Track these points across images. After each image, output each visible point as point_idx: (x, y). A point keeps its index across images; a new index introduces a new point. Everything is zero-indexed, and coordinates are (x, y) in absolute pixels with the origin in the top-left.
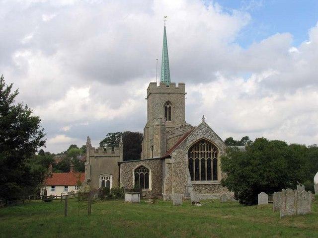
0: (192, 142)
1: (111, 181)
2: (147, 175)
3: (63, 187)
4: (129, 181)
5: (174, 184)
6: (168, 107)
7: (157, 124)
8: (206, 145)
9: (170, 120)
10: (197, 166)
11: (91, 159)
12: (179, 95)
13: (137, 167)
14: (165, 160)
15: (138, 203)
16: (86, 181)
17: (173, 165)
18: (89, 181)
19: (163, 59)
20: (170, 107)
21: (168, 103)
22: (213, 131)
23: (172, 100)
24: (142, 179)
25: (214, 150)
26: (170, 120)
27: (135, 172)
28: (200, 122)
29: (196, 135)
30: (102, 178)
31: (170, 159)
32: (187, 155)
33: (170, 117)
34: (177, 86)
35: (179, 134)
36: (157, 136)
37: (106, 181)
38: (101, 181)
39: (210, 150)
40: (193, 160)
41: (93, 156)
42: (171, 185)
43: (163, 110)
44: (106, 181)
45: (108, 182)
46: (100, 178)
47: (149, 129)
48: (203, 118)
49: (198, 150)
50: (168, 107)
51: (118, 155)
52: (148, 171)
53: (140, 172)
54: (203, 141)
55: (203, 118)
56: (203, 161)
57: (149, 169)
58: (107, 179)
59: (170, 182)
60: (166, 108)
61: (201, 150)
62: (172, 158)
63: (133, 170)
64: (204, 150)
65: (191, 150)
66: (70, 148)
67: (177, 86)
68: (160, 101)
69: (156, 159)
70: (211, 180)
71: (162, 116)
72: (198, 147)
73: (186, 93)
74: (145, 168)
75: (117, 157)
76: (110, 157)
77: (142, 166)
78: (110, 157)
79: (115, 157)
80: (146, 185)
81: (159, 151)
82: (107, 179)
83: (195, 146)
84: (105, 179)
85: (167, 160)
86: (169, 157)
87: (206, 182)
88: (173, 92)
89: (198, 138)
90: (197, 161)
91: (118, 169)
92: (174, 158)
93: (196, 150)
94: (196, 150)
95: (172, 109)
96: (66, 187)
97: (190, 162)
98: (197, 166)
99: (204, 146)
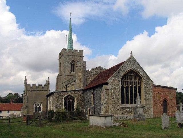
0: (124, 72)
1: (42, 107)
2: (73, 102)
3: (7, 111)
4: (60, 106)
5: (111, 107)
6: (73, 64)
7: (80, 65)
8: (133, 75)
9: (74, 71)
10: (127, 92)
11: (27, 92)
12: (80, 57)
13: (66, 96)
14: (102, 86)
15: (111, 127)
16: (24, 106)
17: (110, 91)
18: (27, 107)
19: (70, 35)
20: (74, 64)
21: (73, 61)
22: (139, 64)
23: (75, 60)
24: (69, 104)
25: (139, 80)
26: (74, 71)
27: (65, 99)
28: (129, 56)
29: (127, 67)
30: (35, 105)
31: (106, 86)
32: (120, 82)
33: (74, 70)
34: (78, 52)
35: (95, 73)
36: (80, 74)
37: (38, 107)
38: (34, 107)
39: (136, 80)
40: (133, 87)
41: (29, 90)
42: (108, 108)
43: (70, 65)
44: (38, 107)
45: (40, 108)
46: (34, 105)
47: (62, 76)
48: (131, 54)
49: (128, 79)
50: (73, 64)
51: (47, 90)
52: (74, 99)
53: (68, 99)
54: (131, 71)
55: (131, 54)
56: (131, 87)
57: (75, 97)
58: (39, 105)
59: (107, 105)
60: (72, 64)
61: (130, 79)
62: (109, 85)
63: (63, 98)
64: (132, 79)
65: (122, 79)
66: (9, 94)
67: (78, 52)
68: (68, 60)
69: (80, 90)
70: (133, 103)
71: (70, 69)
72: (128, 77)
73: (83, 56)
74: (71, 97)
75: (46, 91)
76: (41, 91)
77: (69, 95)
78: (41, 91)
79: (44, 91)
80: (72, 109)
81: (82, 85)
82: (39, 105)
83: (126, 76)
84: (37, 105)
85: (104, 87)
86: (107, 84)
87: (129, 105)
88: (76, 55)
89: (129, 68)
90: (127, 87)
91: (46, 99)
92: (111, 85)
93: (126, 79)
94: (126, 79)
95: (75, 65)
96: (8, 111)
97: (123, 88)
98: (127, 92)
99: (132, 75)
